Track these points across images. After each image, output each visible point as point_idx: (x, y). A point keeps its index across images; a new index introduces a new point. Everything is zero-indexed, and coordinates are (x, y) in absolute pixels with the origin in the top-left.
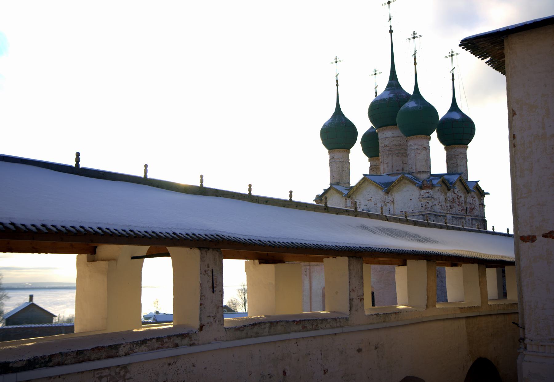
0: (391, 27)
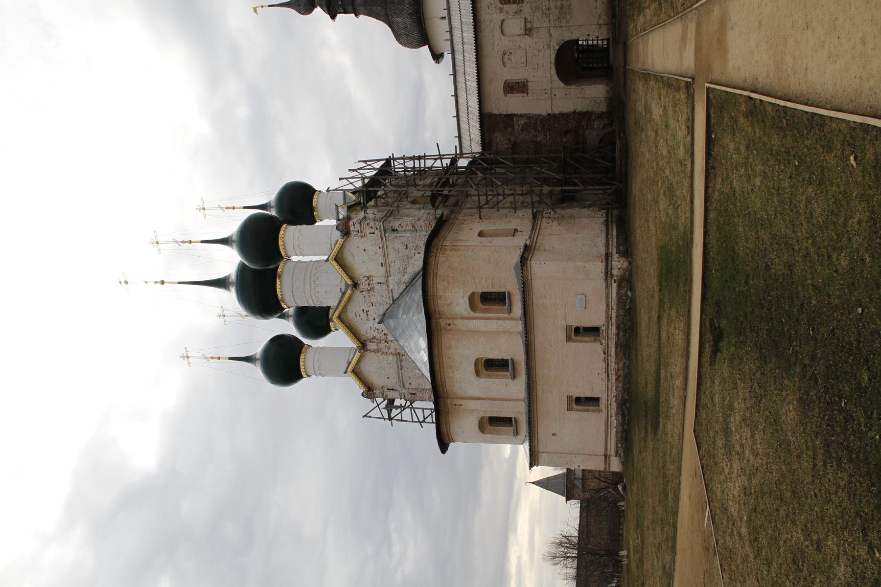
0: (156, 282)
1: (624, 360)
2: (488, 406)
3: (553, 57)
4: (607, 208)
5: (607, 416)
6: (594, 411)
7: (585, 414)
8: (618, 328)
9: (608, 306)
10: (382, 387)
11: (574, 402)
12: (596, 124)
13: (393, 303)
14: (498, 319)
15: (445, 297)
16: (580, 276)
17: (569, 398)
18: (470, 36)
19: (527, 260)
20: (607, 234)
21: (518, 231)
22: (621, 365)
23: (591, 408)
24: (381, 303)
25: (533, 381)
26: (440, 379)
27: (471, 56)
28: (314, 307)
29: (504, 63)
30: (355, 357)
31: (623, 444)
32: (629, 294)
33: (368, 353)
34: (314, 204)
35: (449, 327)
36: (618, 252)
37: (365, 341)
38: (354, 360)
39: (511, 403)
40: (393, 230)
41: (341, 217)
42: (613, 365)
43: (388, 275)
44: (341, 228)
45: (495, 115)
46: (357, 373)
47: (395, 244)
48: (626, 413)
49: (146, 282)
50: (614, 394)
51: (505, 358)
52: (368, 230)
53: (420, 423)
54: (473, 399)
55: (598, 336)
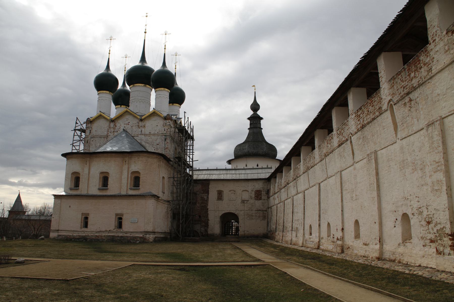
0: (146, 29)
1: (106, 239)
2: (85, 177)
3: (232, 212)
4: (170, 233)
5: (78, 232)
6: (81, 225)
7: (80, 221)
8: (122, 237)
9: (132, 232)
10: (92, 128)
11: (86, 216)
12: (203, 229)
13: (132, 136)
14: (127, 184)
15: (139, 161)
16: (146, 220)
17: (88, 214)
18: (243, 177)
19: (154, 198)
20: (161, 233)
21: (164, 194)
22: (104, 238)
23: (82, 224)
24: (132, 131)
25: (97, 198)
26: (100, 155)
27: (234, 177)
28: (129, 100)
29: (230, 191)
30: (106, 116)
31: (64, 238)
32: (138, 242)
33: (109, 123)
34: (175, 104)
35: (124, 161)
36: (156, 237)
37: (115, 122)
38: (105, 115)
39: (86, 188)
40: (166, 139)
41: (172, 116)
42: (104, 234)
43: (145, 135)
44: (168, 116)
45: (209, 186)
46: (100, 117)
47: (159, 140)
48: (80, 240)
49: (146, 25)
50: (89, 235)
51: (109, 186)
52: (166, 128)
53: (73, 144)
54: (89, 170)
55: (117, 228)
